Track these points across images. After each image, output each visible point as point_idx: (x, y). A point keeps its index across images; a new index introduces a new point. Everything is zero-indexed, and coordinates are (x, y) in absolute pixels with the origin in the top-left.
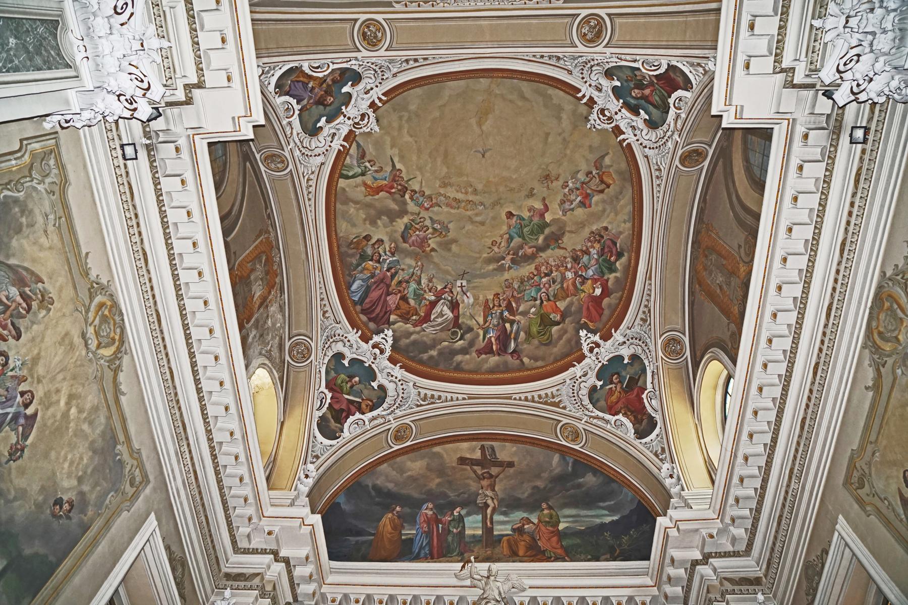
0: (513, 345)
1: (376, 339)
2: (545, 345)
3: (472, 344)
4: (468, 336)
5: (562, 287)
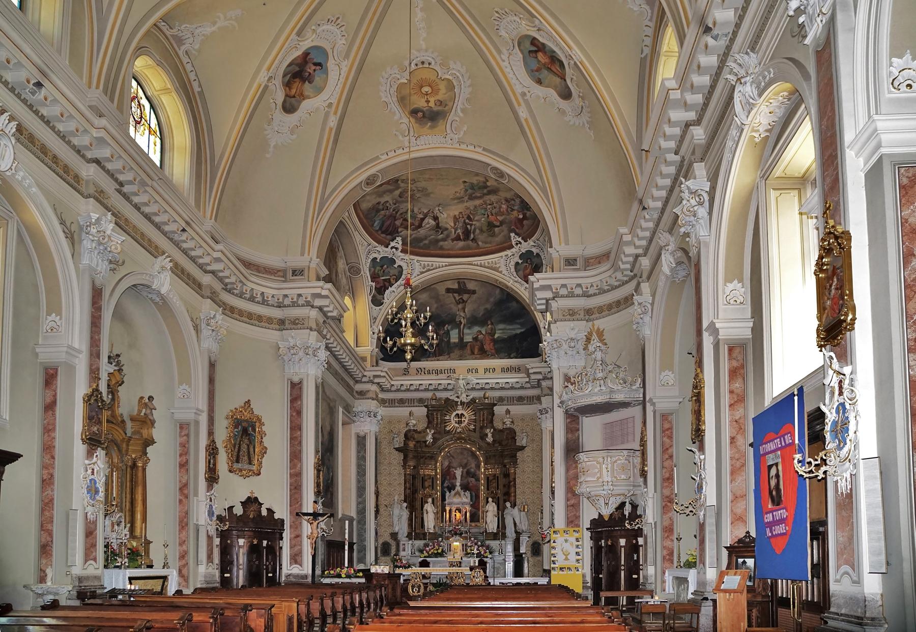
0: (472, 236)
1: (392, 244)
2: (492, 236)
3: (448, 236)
4: (445, 233)
5: (500, 211)
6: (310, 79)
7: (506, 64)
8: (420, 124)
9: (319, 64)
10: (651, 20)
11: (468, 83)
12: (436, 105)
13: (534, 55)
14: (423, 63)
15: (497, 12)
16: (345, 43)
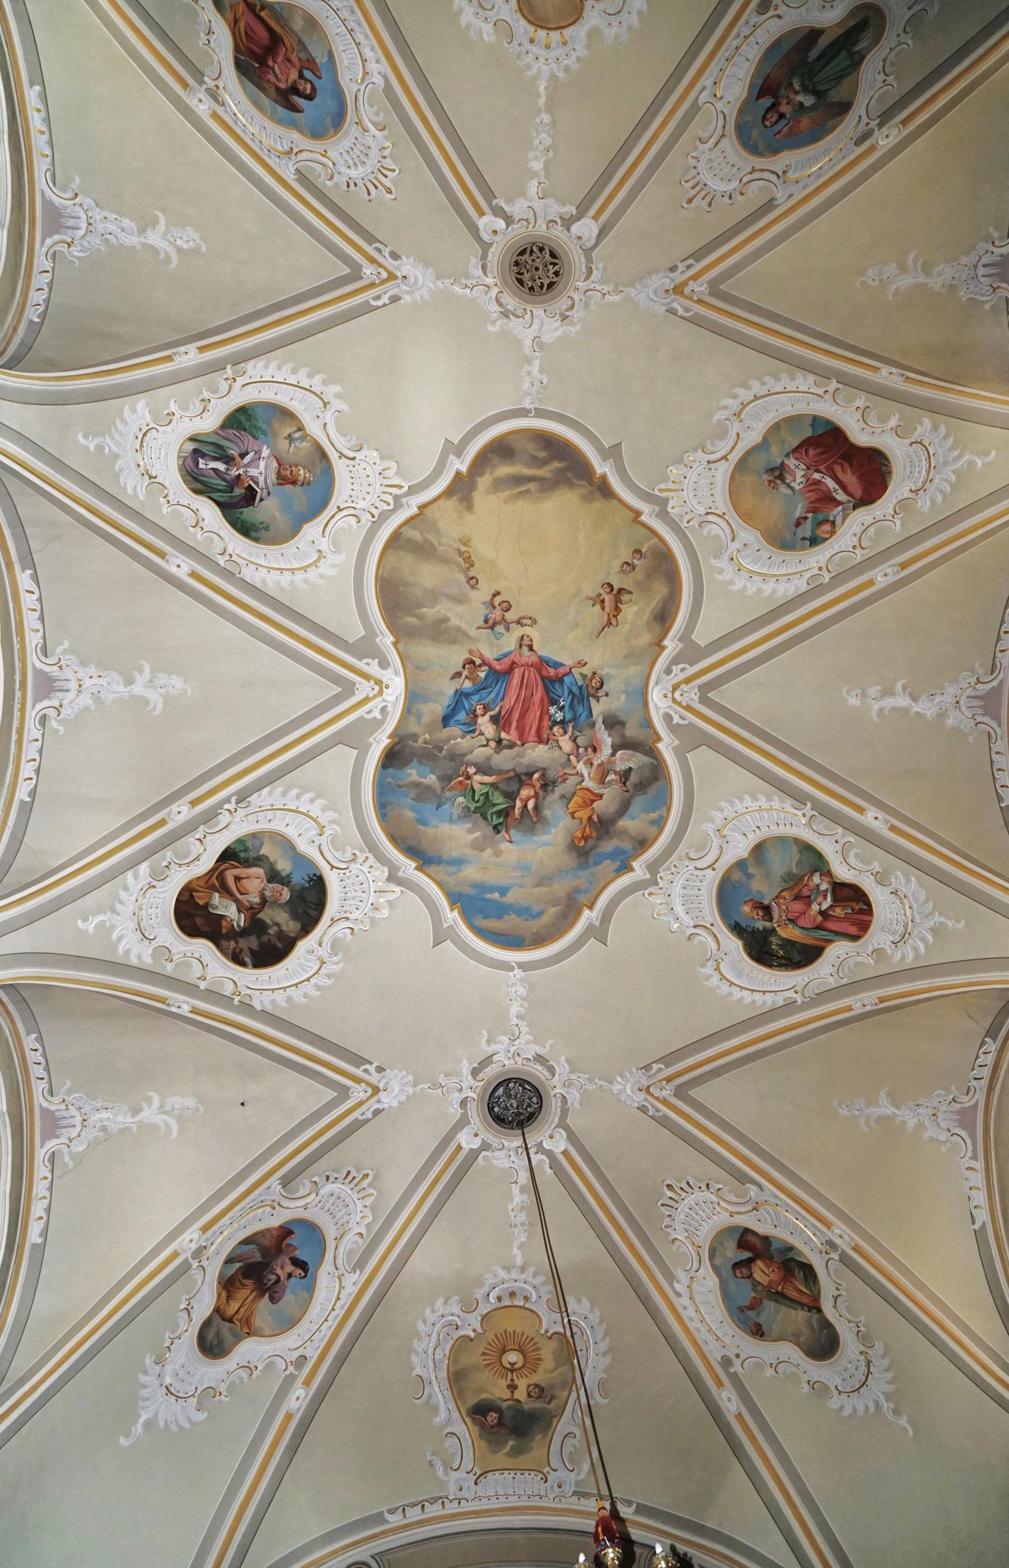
6: (272, 1291)
7: (685, 1301)
8: (490, 1442)
9: (301, 1265)
10: (974, 1157)
11: (604, 1346)
12: (529, 1396)
13: (745, 1271)
14: (512, 1294)
15: (669, 1187)
16: (364, 1231)
